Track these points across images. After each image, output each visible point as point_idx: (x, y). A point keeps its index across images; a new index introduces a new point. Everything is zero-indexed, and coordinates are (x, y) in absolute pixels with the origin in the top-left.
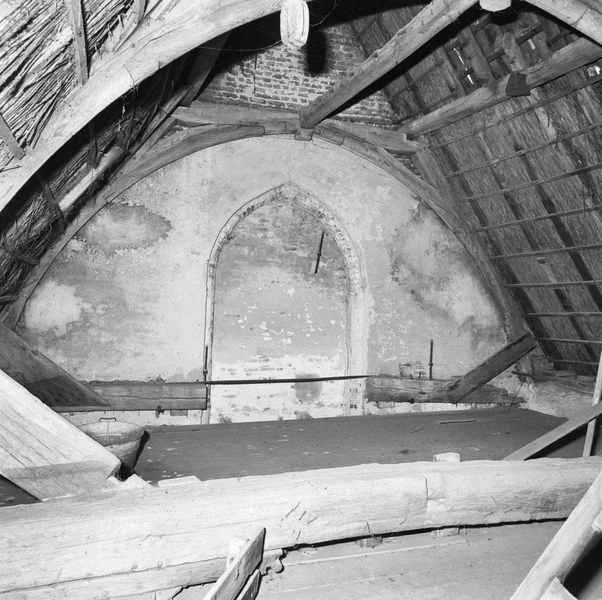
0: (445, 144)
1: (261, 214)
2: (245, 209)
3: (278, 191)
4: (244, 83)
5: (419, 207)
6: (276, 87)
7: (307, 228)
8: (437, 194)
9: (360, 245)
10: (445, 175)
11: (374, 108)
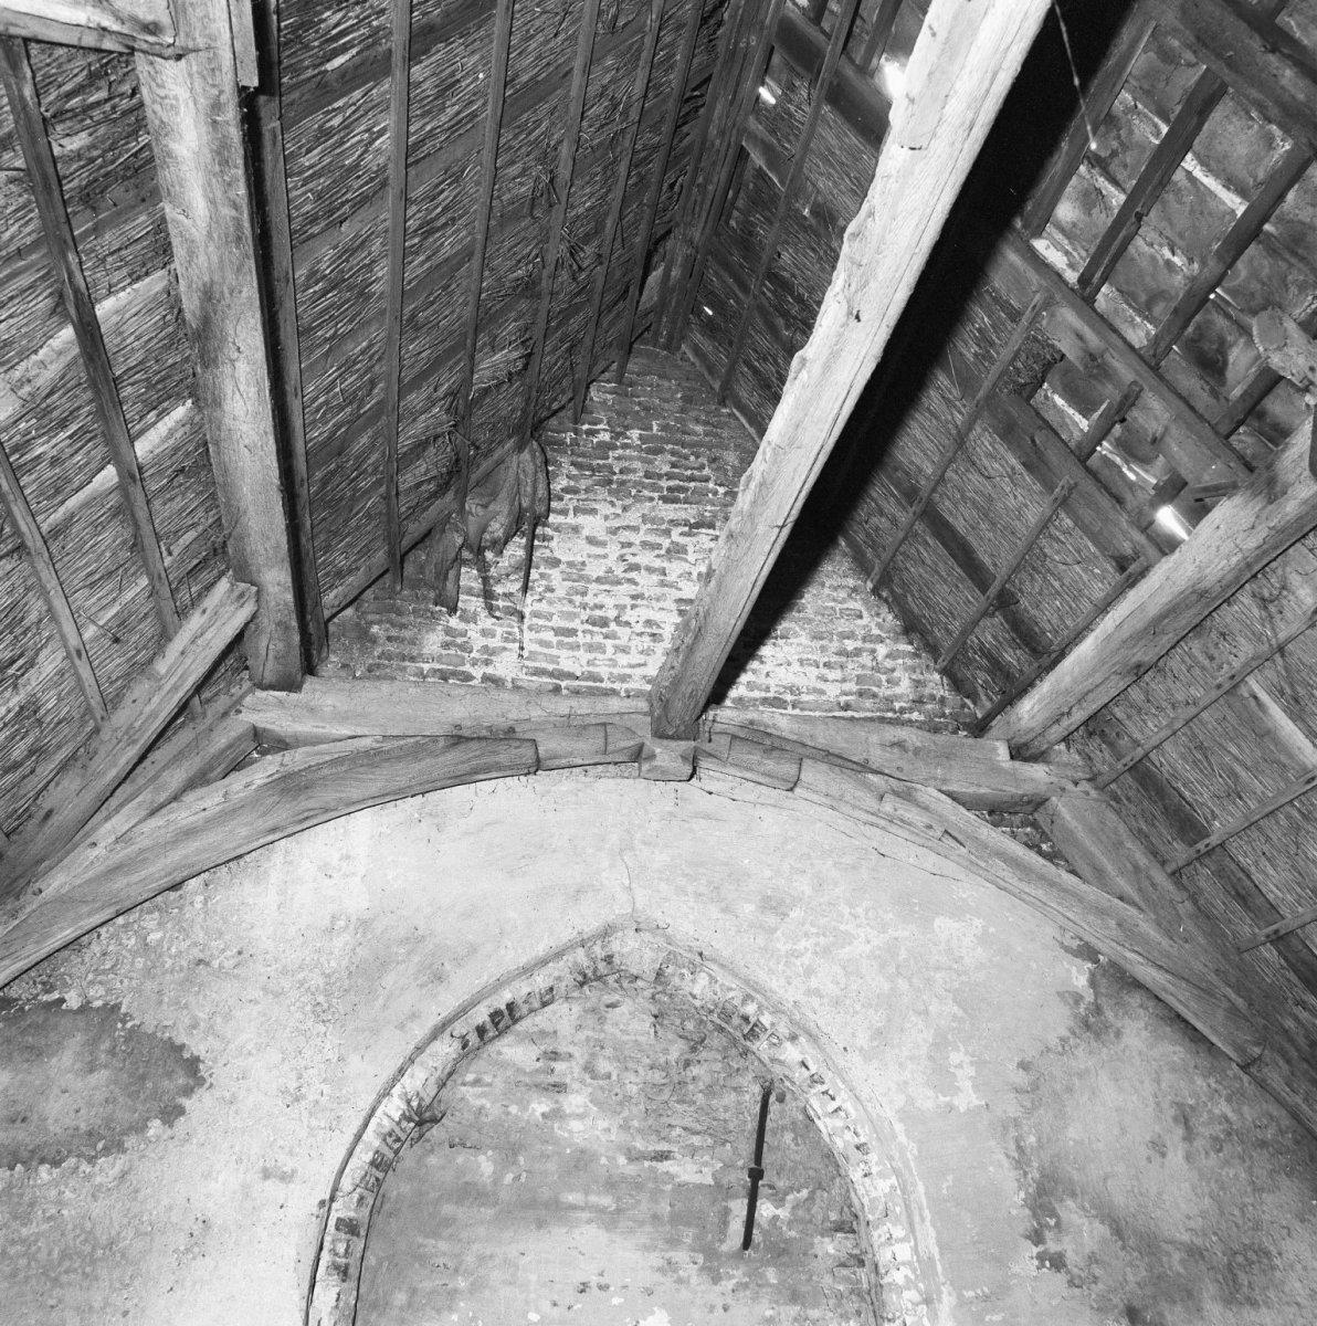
0: (1140, 752)
1: (543, 1034)
2: (481, 1015)
3: (598, 951)
4: (494, 643)
5: (1093, 983)
6: (591, 648)
7: (707, 1079)
8: (1147, 927)
9: (899, 1127)
10: (1163, 863)
11: (898, 690)
